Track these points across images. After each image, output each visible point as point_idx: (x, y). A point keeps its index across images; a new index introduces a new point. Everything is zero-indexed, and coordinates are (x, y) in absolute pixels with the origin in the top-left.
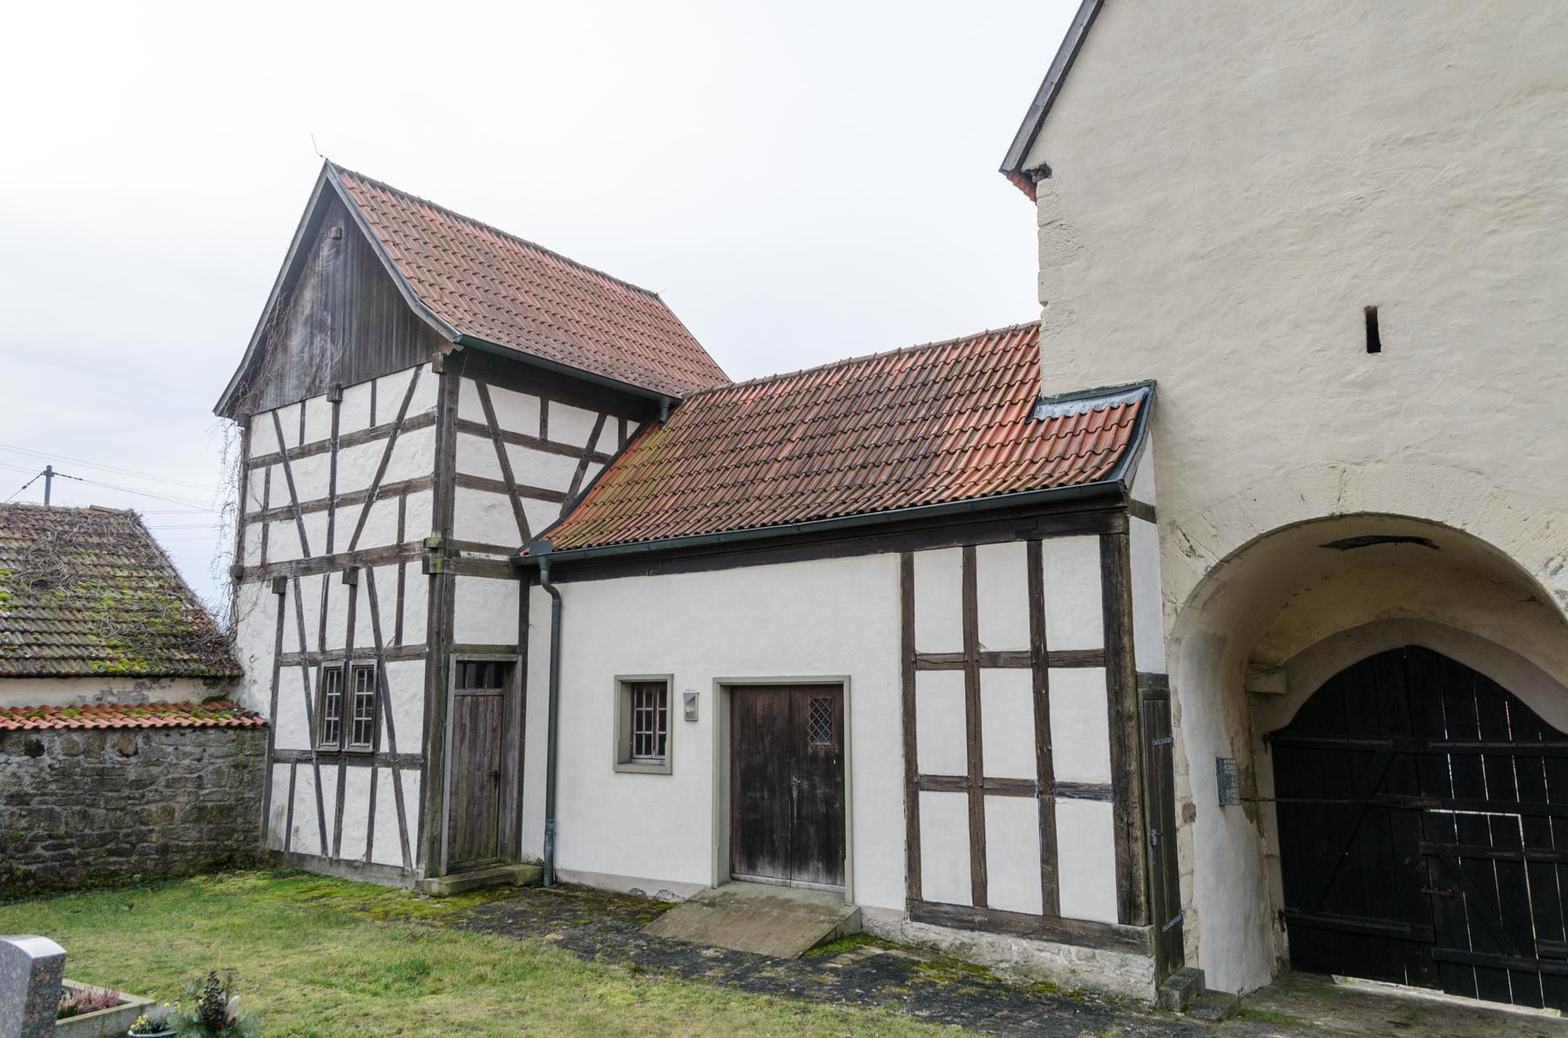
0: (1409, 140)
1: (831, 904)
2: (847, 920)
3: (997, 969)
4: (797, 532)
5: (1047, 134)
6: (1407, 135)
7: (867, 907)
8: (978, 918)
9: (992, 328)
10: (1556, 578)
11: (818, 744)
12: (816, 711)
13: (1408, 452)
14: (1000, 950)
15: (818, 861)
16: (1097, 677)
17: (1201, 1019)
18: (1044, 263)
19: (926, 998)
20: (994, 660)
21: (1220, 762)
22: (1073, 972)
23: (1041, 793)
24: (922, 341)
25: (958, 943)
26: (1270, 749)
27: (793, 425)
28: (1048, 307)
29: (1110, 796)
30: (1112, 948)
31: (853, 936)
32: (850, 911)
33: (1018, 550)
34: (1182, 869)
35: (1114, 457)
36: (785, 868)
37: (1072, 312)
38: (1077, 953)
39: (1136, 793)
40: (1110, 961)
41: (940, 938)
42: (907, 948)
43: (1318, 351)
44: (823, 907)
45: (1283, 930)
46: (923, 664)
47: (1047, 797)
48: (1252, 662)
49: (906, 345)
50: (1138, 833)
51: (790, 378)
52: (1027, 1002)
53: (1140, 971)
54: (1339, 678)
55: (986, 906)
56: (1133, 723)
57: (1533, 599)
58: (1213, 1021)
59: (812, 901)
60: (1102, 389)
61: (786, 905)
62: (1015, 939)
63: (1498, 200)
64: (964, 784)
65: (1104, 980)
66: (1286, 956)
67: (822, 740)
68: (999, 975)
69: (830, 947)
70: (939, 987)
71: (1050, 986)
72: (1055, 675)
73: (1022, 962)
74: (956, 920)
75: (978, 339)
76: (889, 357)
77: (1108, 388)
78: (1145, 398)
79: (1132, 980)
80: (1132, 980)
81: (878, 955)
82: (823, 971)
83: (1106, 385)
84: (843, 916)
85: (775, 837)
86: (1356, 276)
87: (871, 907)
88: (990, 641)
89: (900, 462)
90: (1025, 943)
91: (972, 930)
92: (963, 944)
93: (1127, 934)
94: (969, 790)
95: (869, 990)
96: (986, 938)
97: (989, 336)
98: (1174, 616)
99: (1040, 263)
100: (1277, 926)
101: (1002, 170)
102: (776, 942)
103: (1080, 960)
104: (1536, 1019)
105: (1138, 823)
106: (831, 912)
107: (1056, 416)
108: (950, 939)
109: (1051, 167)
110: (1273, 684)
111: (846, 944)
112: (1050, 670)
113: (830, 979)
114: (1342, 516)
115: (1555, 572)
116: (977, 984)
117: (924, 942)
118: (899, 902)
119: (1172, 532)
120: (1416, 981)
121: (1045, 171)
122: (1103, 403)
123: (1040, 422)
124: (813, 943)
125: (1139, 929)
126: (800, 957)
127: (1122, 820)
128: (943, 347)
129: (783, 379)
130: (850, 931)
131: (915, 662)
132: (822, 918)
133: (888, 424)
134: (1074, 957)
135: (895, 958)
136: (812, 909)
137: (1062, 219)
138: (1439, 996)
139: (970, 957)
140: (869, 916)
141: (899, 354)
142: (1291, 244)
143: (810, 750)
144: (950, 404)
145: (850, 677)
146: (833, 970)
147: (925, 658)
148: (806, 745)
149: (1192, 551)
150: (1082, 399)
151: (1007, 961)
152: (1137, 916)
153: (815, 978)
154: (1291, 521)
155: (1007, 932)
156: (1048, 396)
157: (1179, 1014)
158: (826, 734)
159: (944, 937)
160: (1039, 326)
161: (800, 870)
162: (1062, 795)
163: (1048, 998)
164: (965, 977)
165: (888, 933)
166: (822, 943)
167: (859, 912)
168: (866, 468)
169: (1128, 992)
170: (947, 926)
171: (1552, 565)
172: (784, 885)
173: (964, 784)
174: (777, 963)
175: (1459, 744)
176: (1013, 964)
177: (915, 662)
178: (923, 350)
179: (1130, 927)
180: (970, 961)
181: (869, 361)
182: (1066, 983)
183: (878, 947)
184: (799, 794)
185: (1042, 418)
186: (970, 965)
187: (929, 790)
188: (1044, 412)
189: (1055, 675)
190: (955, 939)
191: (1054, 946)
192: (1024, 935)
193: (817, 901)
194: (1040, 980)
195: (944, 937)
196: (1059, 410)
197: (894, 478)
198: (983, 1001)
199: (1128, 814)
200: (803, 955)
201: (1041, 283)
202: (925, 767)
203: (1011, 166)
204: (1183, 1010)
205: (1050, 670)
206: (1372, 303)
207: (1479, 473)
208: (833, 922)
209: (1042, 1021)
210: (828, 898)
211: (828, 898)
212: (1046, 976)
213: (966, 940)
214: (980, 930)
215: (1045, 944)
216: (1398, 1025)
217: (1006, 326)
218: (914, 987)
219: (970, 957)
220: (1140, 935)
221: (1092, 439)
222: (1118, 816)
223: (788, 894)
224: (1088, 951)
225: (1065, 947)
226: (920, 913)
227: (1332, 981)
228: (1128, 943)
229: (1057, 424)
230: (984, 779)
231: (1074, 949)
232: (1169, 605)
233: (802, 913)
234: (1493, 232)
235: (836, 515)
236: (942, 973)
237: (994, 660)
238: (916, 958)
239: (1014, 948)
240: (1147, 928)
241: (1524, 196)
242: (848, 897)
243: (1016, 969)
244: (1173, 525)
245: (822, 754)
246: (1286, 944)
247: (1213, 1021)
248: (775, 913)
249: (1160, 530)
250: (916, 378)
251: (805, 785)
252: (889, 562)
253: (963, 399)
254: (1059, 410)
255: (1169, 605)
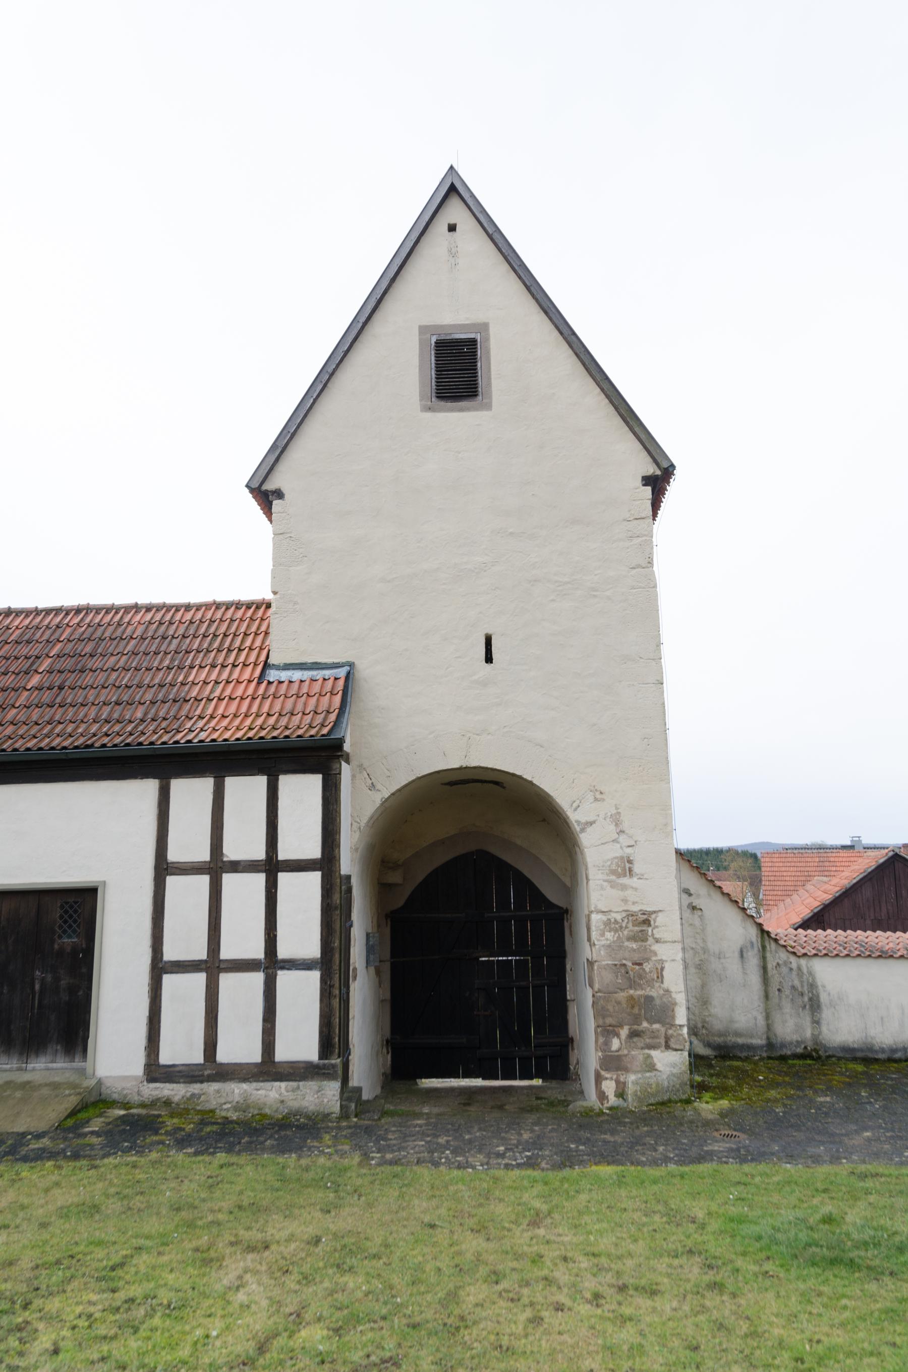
0: (511, 533)
1: (71, 1079)
2: (90, 1091)
3: (221, 1110)
4: (64, 757)
5: (282, 467)
6: (511, 530)
7: (107, 1077)
8: (206, 1073)
9: (219, 599)
10: (576, 813)
11: (66, 940)
12: (66, 912)
13: (506, 730)
14: (225, 1095)
15: (57, 1044)
16: (314, 879)
17: (369, 1120)
18: (277, 563)
19: (183, 1140)
20: (236, 867)
21: (368, 935)
22: (282, 1102)
23: (266, 968)
24: (157, 600)
25: (188, 1094)
26: (389, 923)
27: (37, 657)
28: (278, 596)
29: (319, 966)
30: (312, 1079)
31: (95, 1104)
32: (93, 1082)
33: (260, 782)
34: (350, 1017)
35: (333, 717)
36: (21, 1054)
37: (296, 603)
38: (286, 1087)
39: (338, 962)
40: (311, 1089)
41: (173, 1093)
42: (143, 1105)
43: (459, 657)
44: (64, 1083)
45: (388, 1053)
46: (174, 870)
47: (270, 971)
48: (383, 861)
49: (143, 600)
50: (336, 992)
51: (27, 613)
52: (256, 1129)
53: (332, 1093)
54: (435, 873)
55: (215, 1061)
56: (338, 912)
57: (544, 820)
58: (376, 1120)
59: (51, 1079)
60: (316, 663)
61: (25, 1085)
62: (236, 1084)
63: (556, 582)
64: (203, 966)
65: (305, 1104)
66: (389, 1071)
67: (70, 937)
68: (224, 1114)
69: (80, 1116)
70: (187, 1129)
71: (264, 1116)
72: (283, 878)
73: (242, 1101)
74: (187, 1077)
75: (208, 606)
76: (127, 609)
77: (320, 663)
78: (348, 673)
79: (326, 1100)
80: (326, 1100)
81: (124, 1115)
82: (85, 1135)
83: (319, 661)
84: (88, 1088)
85: (12, 1027)
86: (481, 613)
87: (110, 1077)
88: (231, 852)
89: (153, 703)
90: (245, 1086)
91: (202, 1082)
92: (193, 1095)
93: (324, 1067)
94: (206, 970)
95: (135, 1142)
96: (214, 1086)
97: (218, 605)
98: (358, 833)
99: (274, 562)
100: (385, 1050)
101: (247, 486)
102: (29, 1120)
103: (288, 1091)
104: (531, 1087)
105: (337, 985)
106: (74, 1086)
107: (282, 680)
108: (182, 1092)
109: (284, 492)
110: (395, 878)
111: (91, 1112)
112: (280, 874)
113: (95, 1140)
114: (466, 768)
115: (576, 809)
116: (214, 1123)
117: (158, 1099)
118: (137, 1067)
119: (361, 772)
120: (466, 1075)
121: (279, 494)
122: (319, 674)
123: (270, 683)
124: (66, 1114)
125: (333, 1062)
126: (57, 1128)
127: (326, 983)
128: (178, 608)
129: (18, 613)
130: (92, 1099)
131: (167, 869)
132: (67, 1092)
133: (136, 669)
134: (283, 1090)
135: (139, 1115)
136: (55, 1086)
137: (291, 533)
138: (478, 1082)
139: (198, 1105)
140: (109, 1085)
141: (136, 608)
142: (444, 584)
143: (56, 946)
144: (190, 658)
145: (105, 882)
146: (92, 1133)
147: (176, 865)
148: (53, 942)
149: (373, 787)
150: (302, 669)
151: (230, 1103)
152: (332, 1053)
153: (80, 1141)
154: (437, 769)
155: (231, 1079)
156: (275, 663)
157: (355, 1120)
158: (74, 931)
159: (176, 1091)
160: (269, 606)
161: (37, 1055)
162: (282, 968)
163: (269, 1124)
164: (202, 1120)
165: (125, 1096)
166: (73, 1113)
167: (100, 1082)
168: (120, 704)
169: (322, 1110)
170: (179, 1082)
171: (575, 805)
172: (20, 1069)
173: (203, 966)
174: (39, 1136)
175: (502, 914)
176: (234, 1103)
177: (167, 869)
178: (159, 608)
179: (326, 1061)
180: (198, 1108)
181: (108, 609)
182: (276, 1111)
183: (120, 1108)
184: (41, 986)
185: (271, 680)
186: (199, 1111)
187: (172, 973)
188: (273, 675)
189: (283, 878)
190: (187, 1091)
191: (268, 1085)
192: (245, 1080)
193: (57, 1079)
194: (256, 1112)
195: (176, 1091)
196: (284, 675)
197: (150, 716)
198: (226, 1134)
199: (331, 979)
200: (59, 1125)
201: (273, 577)
202: (170, 954)
203: (255, 485)
204: (356, 1116)
205: (280, 874)
206: (490, 632)
207: (541, 746)
208: (79, 1094)
209: (276, 1140)
210: (67, 1075)
211: (67, 1075)
212: (260, 1109)
213: (196, 1092)
214: (208, 1081)
215: (262, 1084)
216: (465, 1104)
217: (231, 599)
218: (167, 1133)
219: (198, 1105)
220: (334, 1066)
221: (313, 701)
222: (323, 981)
223: (26, 1077)
224: (294, 1084)
225: (277, 1084)
226: (157, 1075)
227: (416, 1084)
228: (324, 1074)
229: (284, 686)
230: (221, 961)
231: (283, 1085)
232: (355, 824)
233: (45, 1091)
234: (553, 600)
235: (104, 746)
236: (183, 1120)
237: (236, 867)
238: (156, 1113)
239: (237, 1090)
240: (339, 1060)
241: (568, 583)
242: (89, 1071)
243: (236, 1108)
244: (361, 767)
245: (68, 949)
246: (389, 1062)
247: (376, 1120)
248: (18, 1094)
249: (352, 770)
250: (156, 631)
251: (49, 978)
252: (149, 788)
253: (202, 654)
254: (284, 675)
255: (355, 824)
